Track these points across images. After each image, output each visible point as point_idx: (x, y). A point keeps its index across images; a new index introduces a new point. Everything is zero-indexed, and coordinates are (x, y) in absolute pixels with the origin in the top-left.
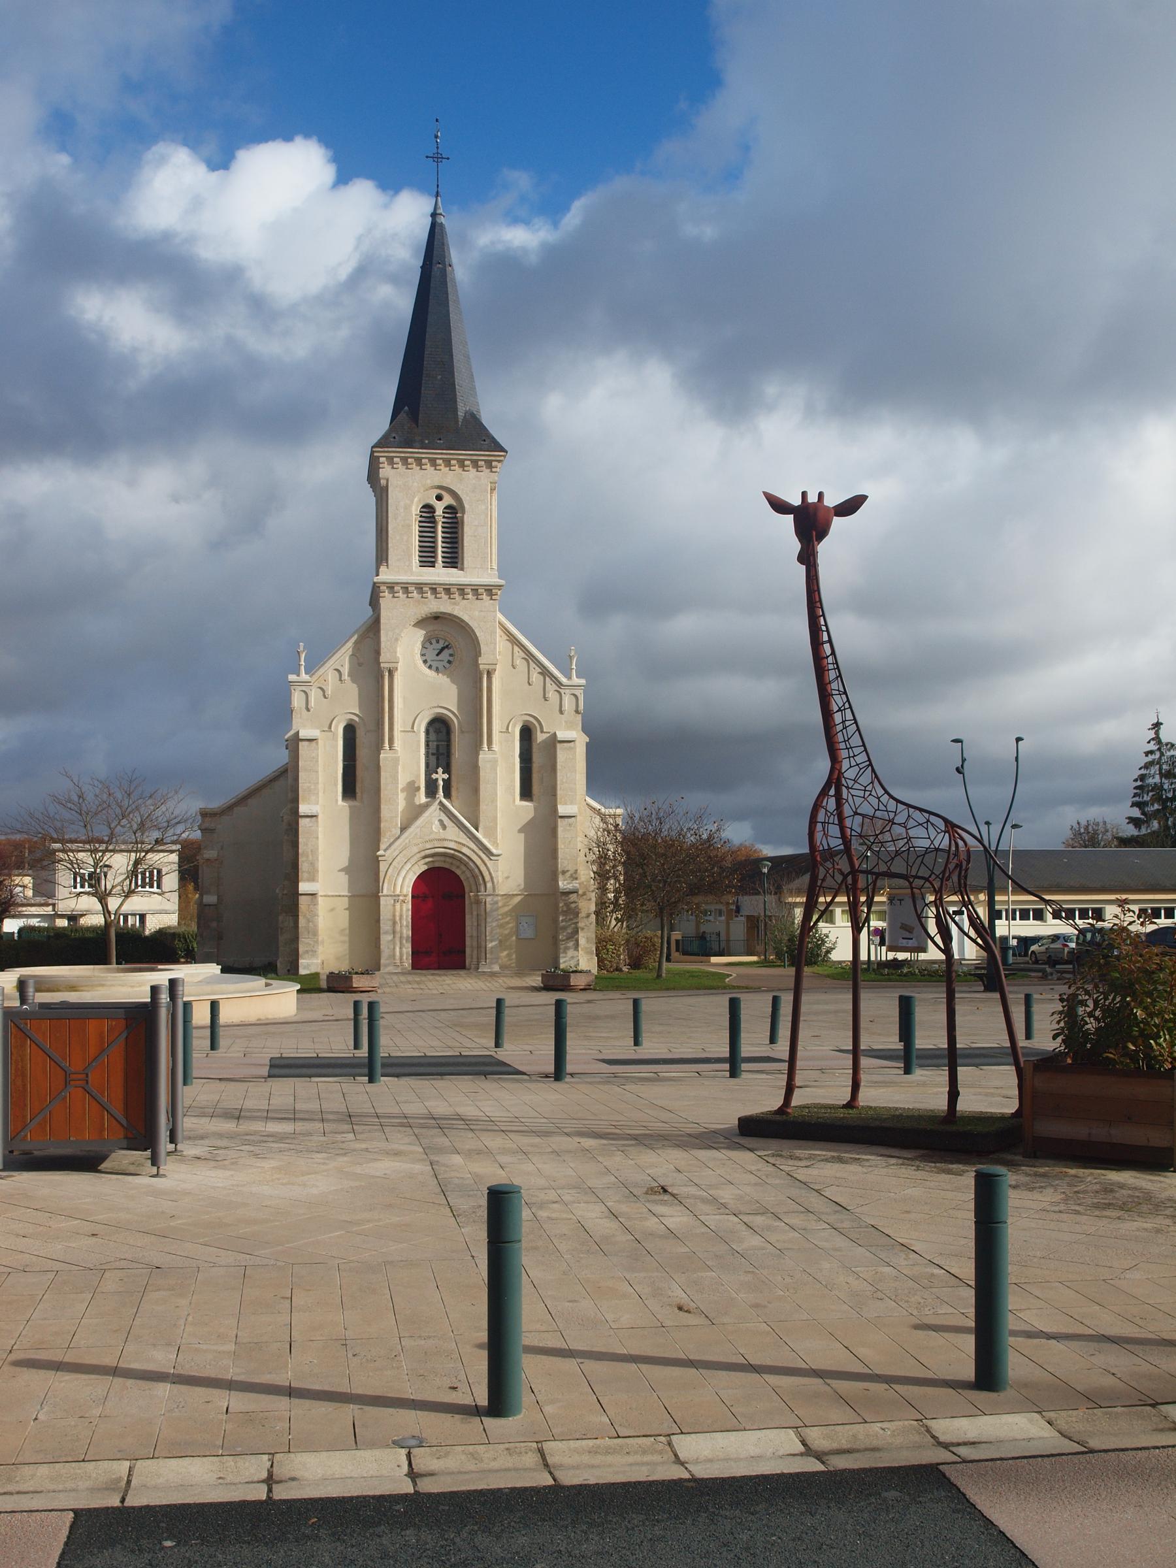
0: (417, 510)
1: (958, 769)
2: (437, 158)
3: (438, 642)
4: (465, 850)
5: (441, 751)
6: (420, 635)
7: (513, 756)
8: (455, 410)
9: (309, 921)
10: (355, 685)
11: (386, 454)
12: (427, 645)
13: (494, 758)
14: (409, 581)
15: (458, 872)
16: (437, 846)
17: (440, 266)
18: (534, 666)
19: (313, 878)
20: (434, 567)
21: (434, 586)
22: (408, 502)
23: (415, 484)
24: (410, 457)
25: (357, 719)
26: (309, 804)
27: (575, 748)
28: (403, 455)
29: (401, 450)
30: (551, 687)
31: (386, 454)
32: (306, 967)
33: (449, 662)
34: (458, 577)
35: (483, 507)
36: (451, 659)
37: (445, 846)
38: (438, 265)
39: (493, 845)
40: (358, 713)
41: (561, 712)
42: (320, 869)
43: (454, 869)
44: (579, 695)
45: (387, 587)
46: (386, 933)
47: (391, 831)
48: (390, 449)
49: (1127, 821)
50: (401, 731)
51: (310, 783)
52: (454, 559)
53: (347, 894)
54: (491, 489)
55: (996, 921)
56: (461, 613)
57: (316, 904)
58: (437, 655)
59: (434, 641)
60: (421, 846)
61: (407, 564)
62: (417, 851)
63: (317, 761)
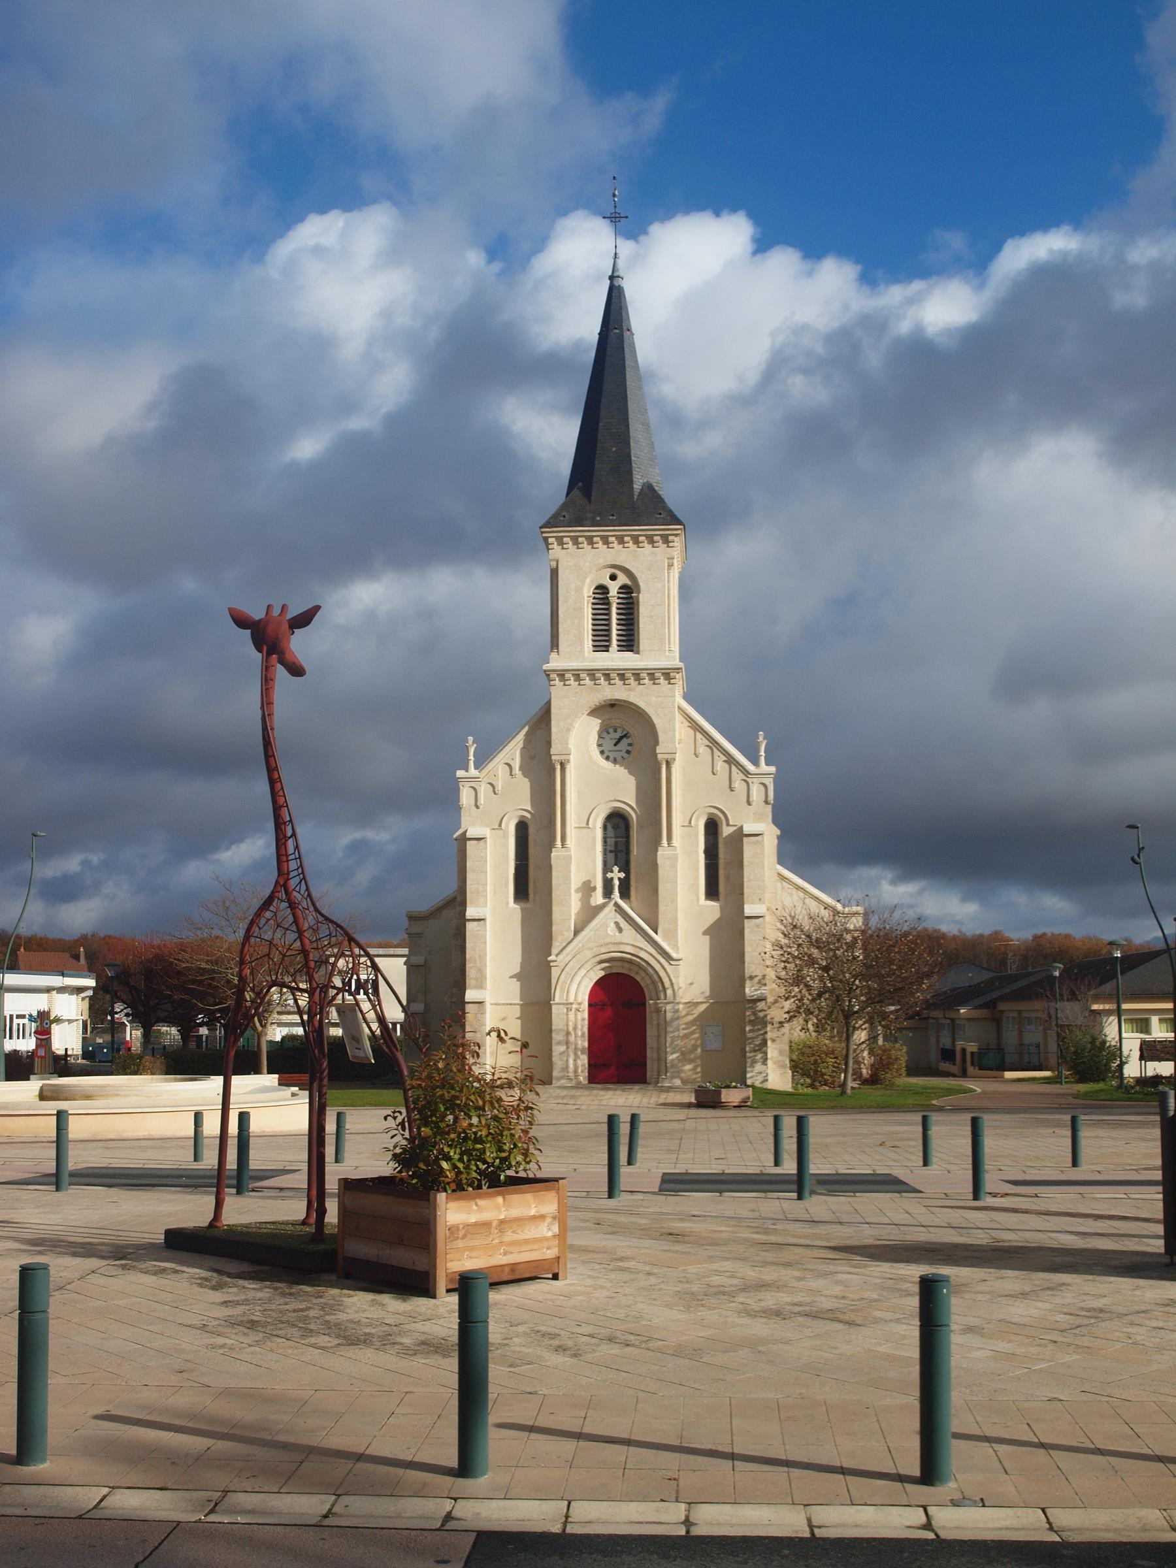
0: (589, 591)
6: (595, 724)
7: (697, 852)
8: (631, 482)
10: (527, 780)
11: (555, 535)
12: (604, 734)
13: (674, 854)
15: (638, 978)
16: (612, 950)
17: (617, 331)
18: (719, 754)
20: (608, 651)
22: (579, 583)
23: (587, 564)
25: (528, 816)
26: (476, 907)
28: (573, 534)
30: (737, 776)
31: (555, 535)
33: (628, 752)
34: (633, 661)
35: (660, 585)
36: (630, 748)
37: (622, 950)
40: (529, 809)
41: (749, 803)
46: (559, 1043)
50: (575, 827)
51: (478, 884)
52: (630, 643)
55: (490, 1293)
56: (638, 699)
57: (483, 1013)
58: (615, 745)
59: (611, 731)
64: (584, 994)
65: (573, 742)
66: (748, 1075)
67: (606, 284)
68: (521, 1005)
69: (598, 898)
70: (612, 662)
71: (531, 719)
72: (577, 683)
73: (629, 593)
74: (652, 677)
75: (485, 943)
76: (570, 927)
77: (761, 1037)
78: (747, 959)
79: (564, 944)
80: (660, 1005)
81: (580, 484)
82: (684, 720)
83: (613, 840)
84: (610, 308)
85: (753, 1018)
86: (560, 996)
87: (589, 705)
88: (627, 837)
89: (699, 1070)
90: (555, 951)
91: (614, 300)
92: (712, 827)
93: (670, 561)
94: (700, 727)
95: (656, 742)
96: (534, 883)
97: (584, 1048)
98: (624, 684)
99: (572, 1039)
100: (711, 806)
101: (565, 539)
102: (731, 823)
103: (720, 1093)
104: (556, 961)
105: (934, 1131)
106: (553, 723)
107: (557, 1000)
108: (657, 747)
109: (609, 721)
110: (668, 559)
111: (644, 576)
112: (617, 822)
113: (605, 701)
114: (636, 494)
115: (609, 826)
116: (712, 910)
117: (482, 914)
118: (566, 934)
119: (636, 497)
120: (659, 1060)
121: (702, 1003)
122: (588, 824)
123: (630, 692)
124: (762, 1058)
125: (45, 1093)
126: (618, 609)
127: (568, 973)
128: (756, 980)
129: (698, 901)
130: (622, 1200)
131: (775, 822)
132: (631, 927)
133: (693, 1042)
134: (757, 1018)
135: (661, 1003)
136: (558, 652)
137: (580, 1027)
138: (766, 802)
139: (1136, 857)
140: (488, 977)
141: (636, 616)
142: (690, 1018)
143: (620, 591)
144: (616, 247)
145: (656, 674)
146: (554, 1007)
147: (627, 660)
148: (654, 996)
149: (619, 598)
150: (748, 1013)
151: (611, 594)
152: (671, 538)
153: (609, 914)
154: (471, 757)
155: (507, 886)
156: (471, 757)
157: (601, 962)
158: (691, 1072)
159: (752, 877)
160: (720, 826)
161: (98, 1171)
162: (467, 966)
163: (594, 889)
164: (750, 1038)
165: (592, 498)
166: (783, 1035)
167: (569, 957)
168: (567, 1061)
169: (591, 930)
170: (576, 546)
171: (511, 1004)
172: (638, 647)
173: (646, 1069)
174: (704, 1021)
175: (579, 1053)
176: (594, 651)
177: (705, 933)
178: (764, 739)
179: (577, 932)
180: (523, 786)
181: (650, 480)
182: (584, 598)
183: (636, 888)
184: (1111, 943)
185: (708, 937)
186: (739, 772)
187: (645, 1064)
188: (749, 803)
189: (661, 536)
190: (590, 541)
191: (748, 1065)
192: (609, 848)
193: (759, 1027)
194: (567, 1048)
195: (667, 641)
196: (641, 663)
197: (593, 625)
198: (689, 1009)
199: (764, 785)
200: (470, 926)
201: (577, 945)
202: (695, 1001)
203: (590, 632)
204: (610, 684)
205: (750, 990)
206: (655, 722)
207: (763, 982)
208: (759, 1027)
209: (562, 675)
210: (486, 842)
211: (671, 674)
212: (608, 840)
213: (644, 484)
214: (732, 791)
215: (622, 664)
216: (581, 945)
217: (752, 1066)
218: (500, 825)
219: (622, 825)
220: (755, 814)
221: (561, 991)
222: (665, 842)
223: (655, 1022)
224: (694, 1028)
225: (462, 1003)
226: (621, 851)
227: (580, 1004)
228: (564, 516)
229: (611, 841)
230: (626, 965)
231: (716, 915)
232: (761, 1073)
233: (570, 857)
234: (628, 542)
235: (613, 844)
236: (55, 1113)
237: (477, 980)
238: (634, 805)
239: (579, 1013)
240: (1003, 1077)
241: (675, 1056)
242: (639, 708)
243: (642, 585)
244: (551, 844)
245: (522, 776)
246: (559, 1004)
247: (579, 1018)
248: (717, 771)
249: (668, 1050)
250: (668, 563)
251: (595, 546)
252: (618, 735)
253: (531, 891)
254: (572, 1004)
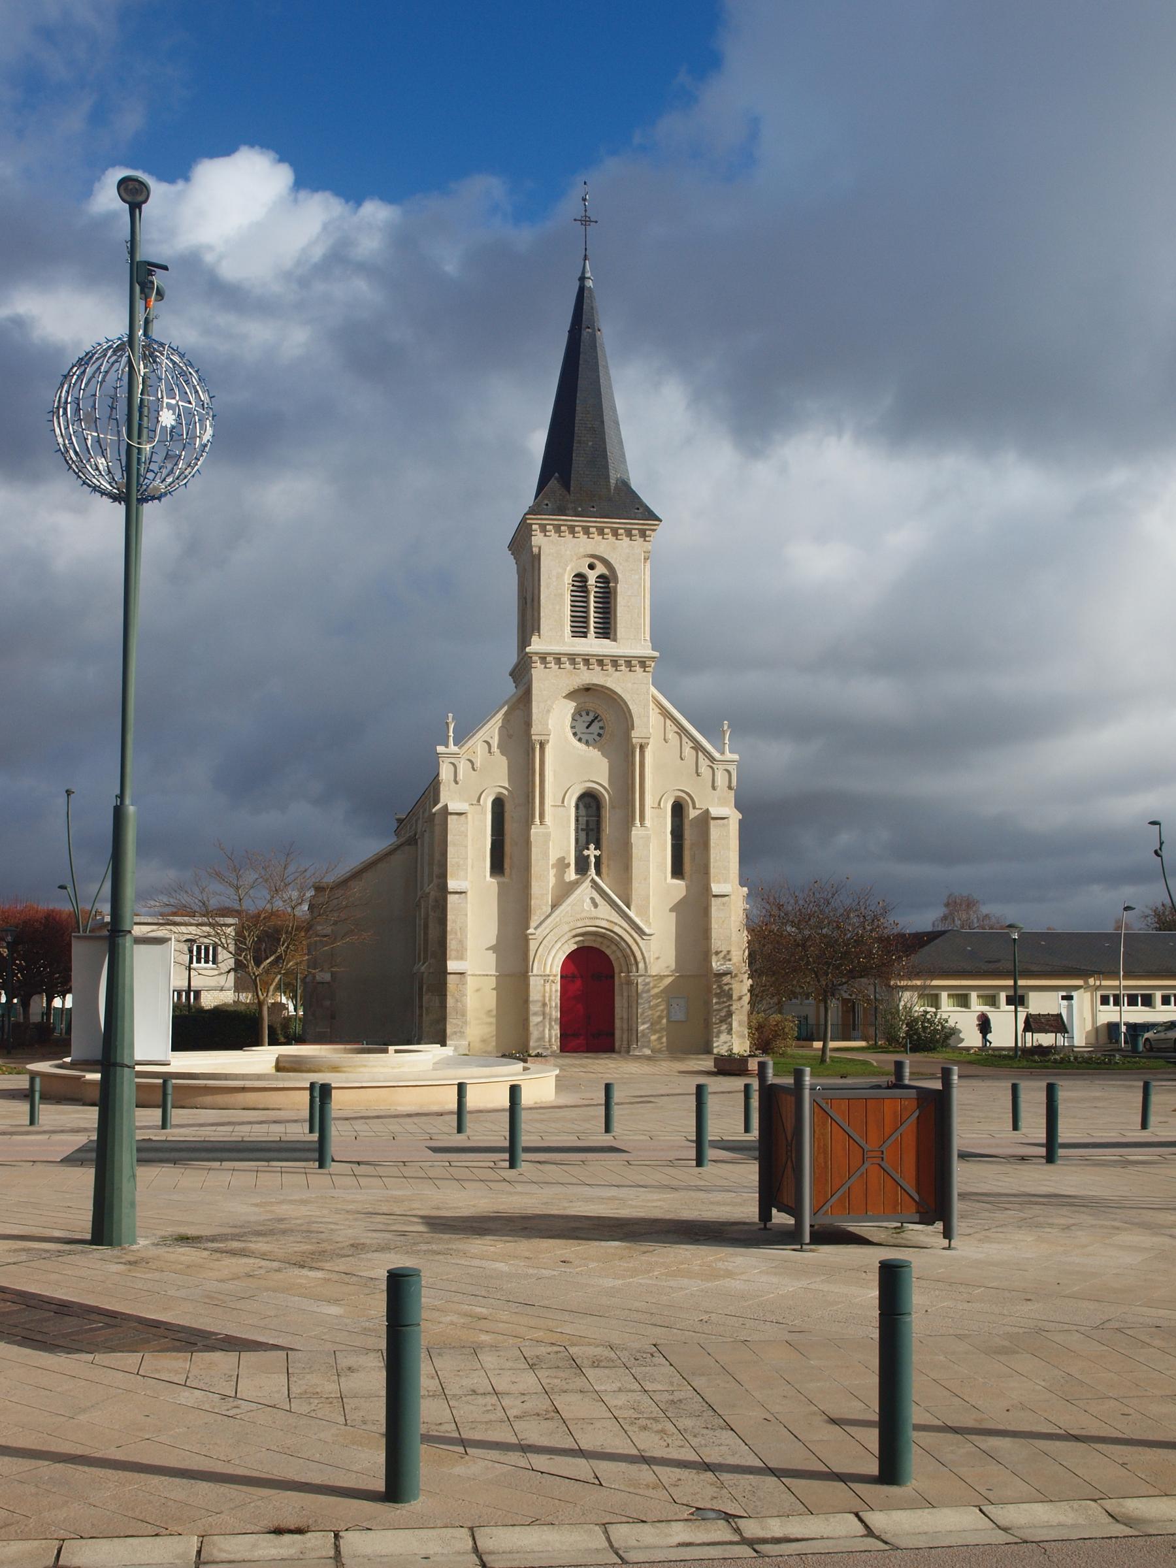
0: (569, 579)
3: (588, 714)
6: (571, 706)
7: (665, 833)
8: (607, 477)
9: (457, 1001)
10: (505, 758)
11: (539, 522)
12: (578, 717)
15: (608, 952)
16: (588, 924)
17: (590, 330)
18: (688, 740)
19: (461, 957)
20: (586, 637)
22: (560, 570)
23: (568, 552)
25: (506, 792)
26: (457, 880)
27: (728, 825)
28: (556, 522)
30: (704, 762)
31: (539, 522)
33: (599, 735)
34: (611, 648)
35: (637, 577)
36: (601, 732)
37: (597, 925)
40: (507, 786)
41: (714, 788)
44: (732, 771)
46: (535, 1014)
51: (458, 858)
52: (607, 630)
53: (494, 973)
57: (465, 984)
58: (587, 728)
59: (584, 713)
62: (568, 929)
64: (557, 966)
65: (552, 723)
66: (715, 1045)
68: (497, 976)
69: (571, 875)
71: (510, 698)
72: (558, 666)
73: (607, 584)
74: (629, 664)
75: (466, 915)
76: (548, 902)
77: (726, 1009)
78: (714, 935)
79: (542, 919)
80: (632, 978)
81: (557, 474)
82: (655, 707)
83: (585, 818)
84: (582, 309)
85: (718, 991)
86: (538, 969)
87: (568, 688)
88: (598, 815)
89: (664, 1040)
90: (533, 924)
91: (586, 301)
92: (678, 809)
94: (669, 713)
95: (633, 728)
96: (511, 858)
97: (556, 1019)
98: (602, 670)
99: (547, 1010)
100: (679, 790)
101: (548, 527)
102: (697, 807)
103: (747, 1061)
104: (535, 934)
105: (1154, 1099)
106: (534, 704)
107: (535, 972)
108: (633, 732)
109: (583, 705)
112: (589, 802)
115: (581, 806)
116: (679, 887)
118: (544, 908)
120: (629, 1030)
121: (668, 976)
122: (563, 802)
123: (607, 678)
124: (726, 1028)
125: (281, 1065)
126: (595, 597)
127: (545, 945)
128: (722, 955)
129: (666, 879)
130: (709, 1169)
131: (738, 806)
132: (605, 903)
133: (658, 1013)
134: (724, 991)
135: (634, 976)
136: (539, 635)
137: (554, 998)
138: (730, 788)
139: (1159, 851)
140: (469, 948)
141: (613, 605)
142: (656, 990)
143: (597, 580)
144: (586, 249)
145: (633, 662)
146: (531, 979)
148: (625, 969)
149: (596, 587)
150: (714, 987)
151: (590, 582)
152: (648, 533)
153: (585, 891)
154: (451, 734)
155: (485, 860)
156: (451, 734)
157: (575, 936)
158: (656, 1042)
160: (686, 808)
161: (264, 1145)
162: (448, 937)
163: (568, 865)
164: (716, 1010)
165: (572, 489)
166: (742, 1007)
167: (548, 930)
168: (544, 1030)
169: (569, 905)
170: (558, 535)
171: (487, 975)
172: (615, 634)
173: (614, 1040)
174: (670, 994)
175: (553, 1023)
177: (671, 910)
178: (729, 727)
179: (554, 906)
180: (501, 764)
183: (608, 866)
184: (1010, 926)
185: (674, 914)
187: (613, 1035)
188: (714, 788)
190: (572, 530)
191: (714, 1034)
192: (580, 827)
193: (725, 999)
194: (544, 1018)
196: (618, 651)
197: (572, 611)
198: (655, 982)
199: (728, 771)
200: (451, 899)
201: (554, 919)
202: (662, 974)
204: (588, 669)
205: (716, 965)
207: (728, 957)
208: (725, 999)
209: (543, 658)
210: (467, 817)
211: (647, 663)
212: (580, 818)
214: (698, 775)
215: (558, 648)
216: (558, 919)
217: (718, 1036)
218: (479, 800)
219: (594, 805)
220: (719, 799)
221: (538, 963)
224: (660, 1000)
225: (443, 972)
226: (592, 830)
227: (555, 976)
228: (547, 505)
229: (583, 820)
230: (599, 939)
231: (682, 893)
232: (725, 1043)
235: (585, 822)
236: (308, 1086)
237: (458, 951)
238: (607, 786)
239: (554, 985)
240: (812, 1046)
241: (646, 1026)
242: (615, 693)
243: (620, 576)
244: (528, 822)
245: (499, 754)
246: (537, 976)
247: (554, 989)
248: (685, 757)
249: (639, 1020)
251: (576, 535)
252: (590, 718)
253: (506, 866)
254: (549, 976)
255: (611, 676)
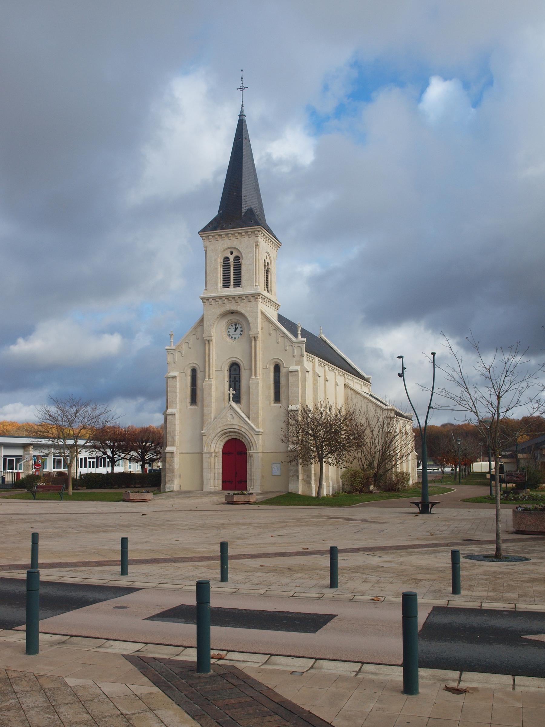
0: (221, 260)
1: (399, 375)
2: (242, 88)
4: (243, 430)
5: (236, 380)
6: (224, 323)
9: (170, 465)
11: (205, 235)
12: (230, 327)
13: (257, 382)
14: (215, 296)
15: (243, 441)
16: (229, 428)
17: (240, 140)
18: (280, 333)
19: (173, 445)
20: (229, 288)
21: (227, 297)
22: (216, 257)
23: (219, 248)
24: (216, 235)
26: (172, 408)
29: (211, 232)
30: (288, 344)
31: (205, 235)
32: (169, 488)
33: (241, 334)
34: (240, 292)
35: (251, 255)
36: (241, 333)
37: (233, 427)
38: (239, 140)
39: (256, 427)
42: (176, 440)
43: (241, 439)
44: (302, 346)
45: (206, 300)
47: (208, 421)
48: (206, 232)
49: (351, 411)
50: (215, 371)
51: (173, 398)
52: (238, 284)
54: (255, 246)
57: (173, 457)
60: (222, 428)
61: (216, 287)
62: (220, 430)
63: (176, 387)
67: (238, 118)
70: (230, 292)
92: (277, 368)
93: (256, 243)
100: (189, 364)
110: (255, 242)
111: (244, 251)
113: (227, 311)
114: (243, 213)
117: (173, 412)
119: (243, 215)
147: (238, 291)
159: (293, 392)
176: (234, 287)
181: (252, 207)
182: (218, 264)
186: (289, 342)
189: (252, 232)
195: (255, 281)
203: (222, 279)
206: (249, 319)
213: (248, 209)
220: (296, 361)
222: (253, 376)
223: (250, 462)
233: (211, 385)
234: (231, 237)
237: (171, 442)
250: (255, 244)
254: (212, 453)
255: (239, 305)
